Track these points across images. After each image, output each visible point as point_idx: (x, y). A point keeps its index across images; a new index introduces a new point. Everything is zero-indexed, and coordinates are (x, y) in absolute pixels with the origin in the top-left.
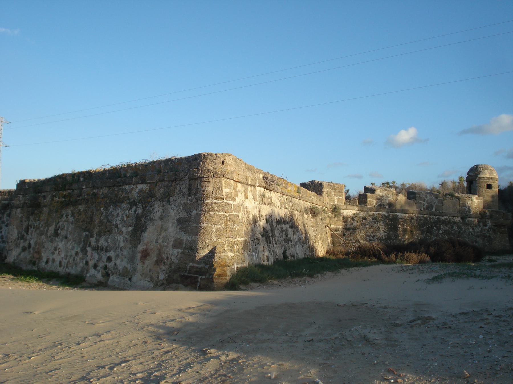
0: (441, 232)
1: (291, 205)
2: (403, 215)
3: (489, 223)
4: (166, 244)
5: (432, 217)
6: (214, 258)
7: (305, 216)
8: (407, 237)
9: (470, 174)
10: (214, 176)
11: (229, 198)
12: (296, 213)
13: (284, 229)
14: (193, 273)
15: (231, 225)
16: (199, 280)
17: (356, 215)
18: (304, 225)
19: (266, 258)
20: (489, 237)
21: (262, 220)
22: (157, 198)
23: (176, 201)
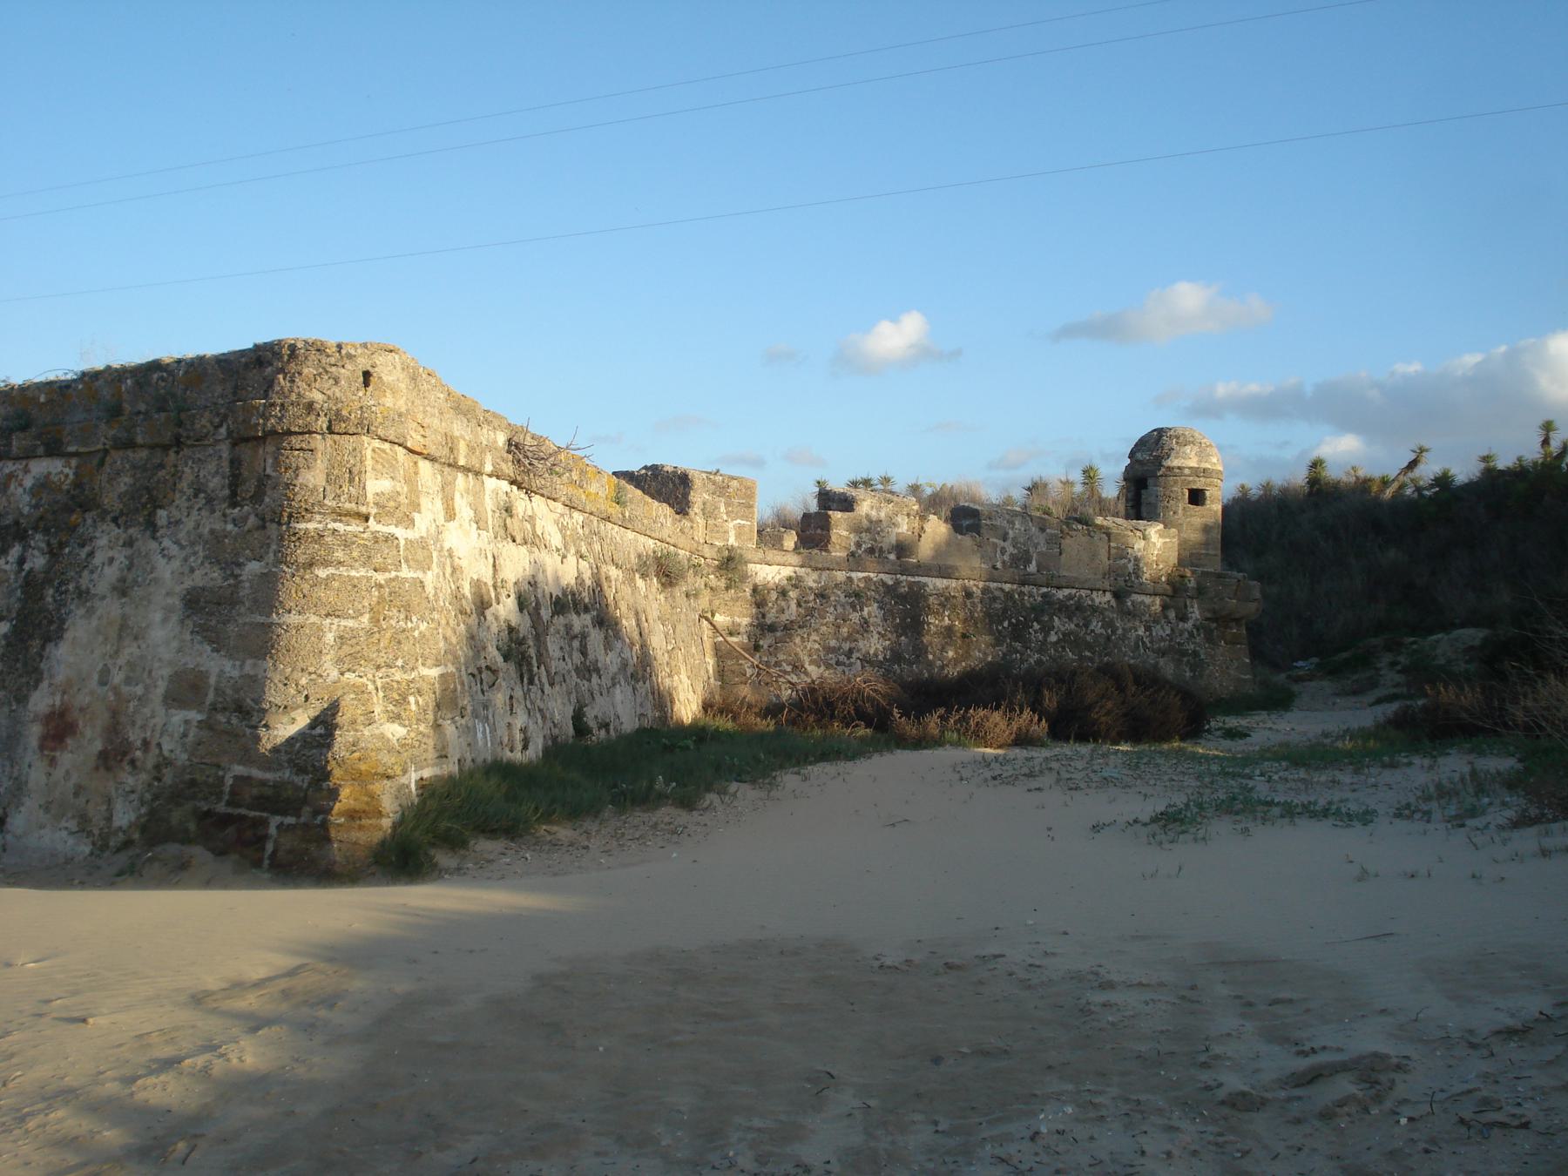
0: (1053, 638)
1: (597, 547)
2: (941, 583)
3: (1195, 612)
4: (139, 690)
5: (1026, 589)
6: (329, 746)
7: (640, 583)
8: (951, 654)
9: (1139, 456)
10: (331, 431)
11: (390, 514)
12: (614, 572)
13: (577, 628)
14: (251, 811)
15: (396, 620)
16: (273, 830)
17: (795, 582)
18: (637, 614)
19: (518, 736)
20: (1195, 654)
21: (503, 598)
22: (106, 512)
23: (178, 522)
